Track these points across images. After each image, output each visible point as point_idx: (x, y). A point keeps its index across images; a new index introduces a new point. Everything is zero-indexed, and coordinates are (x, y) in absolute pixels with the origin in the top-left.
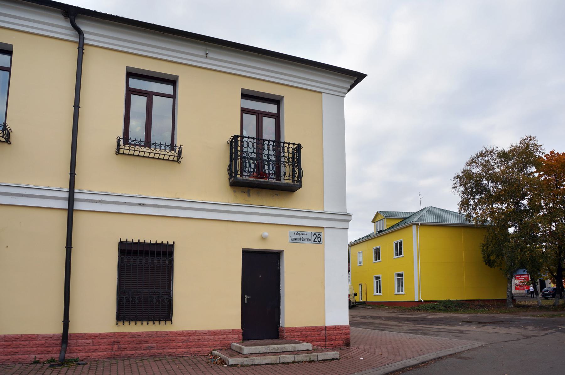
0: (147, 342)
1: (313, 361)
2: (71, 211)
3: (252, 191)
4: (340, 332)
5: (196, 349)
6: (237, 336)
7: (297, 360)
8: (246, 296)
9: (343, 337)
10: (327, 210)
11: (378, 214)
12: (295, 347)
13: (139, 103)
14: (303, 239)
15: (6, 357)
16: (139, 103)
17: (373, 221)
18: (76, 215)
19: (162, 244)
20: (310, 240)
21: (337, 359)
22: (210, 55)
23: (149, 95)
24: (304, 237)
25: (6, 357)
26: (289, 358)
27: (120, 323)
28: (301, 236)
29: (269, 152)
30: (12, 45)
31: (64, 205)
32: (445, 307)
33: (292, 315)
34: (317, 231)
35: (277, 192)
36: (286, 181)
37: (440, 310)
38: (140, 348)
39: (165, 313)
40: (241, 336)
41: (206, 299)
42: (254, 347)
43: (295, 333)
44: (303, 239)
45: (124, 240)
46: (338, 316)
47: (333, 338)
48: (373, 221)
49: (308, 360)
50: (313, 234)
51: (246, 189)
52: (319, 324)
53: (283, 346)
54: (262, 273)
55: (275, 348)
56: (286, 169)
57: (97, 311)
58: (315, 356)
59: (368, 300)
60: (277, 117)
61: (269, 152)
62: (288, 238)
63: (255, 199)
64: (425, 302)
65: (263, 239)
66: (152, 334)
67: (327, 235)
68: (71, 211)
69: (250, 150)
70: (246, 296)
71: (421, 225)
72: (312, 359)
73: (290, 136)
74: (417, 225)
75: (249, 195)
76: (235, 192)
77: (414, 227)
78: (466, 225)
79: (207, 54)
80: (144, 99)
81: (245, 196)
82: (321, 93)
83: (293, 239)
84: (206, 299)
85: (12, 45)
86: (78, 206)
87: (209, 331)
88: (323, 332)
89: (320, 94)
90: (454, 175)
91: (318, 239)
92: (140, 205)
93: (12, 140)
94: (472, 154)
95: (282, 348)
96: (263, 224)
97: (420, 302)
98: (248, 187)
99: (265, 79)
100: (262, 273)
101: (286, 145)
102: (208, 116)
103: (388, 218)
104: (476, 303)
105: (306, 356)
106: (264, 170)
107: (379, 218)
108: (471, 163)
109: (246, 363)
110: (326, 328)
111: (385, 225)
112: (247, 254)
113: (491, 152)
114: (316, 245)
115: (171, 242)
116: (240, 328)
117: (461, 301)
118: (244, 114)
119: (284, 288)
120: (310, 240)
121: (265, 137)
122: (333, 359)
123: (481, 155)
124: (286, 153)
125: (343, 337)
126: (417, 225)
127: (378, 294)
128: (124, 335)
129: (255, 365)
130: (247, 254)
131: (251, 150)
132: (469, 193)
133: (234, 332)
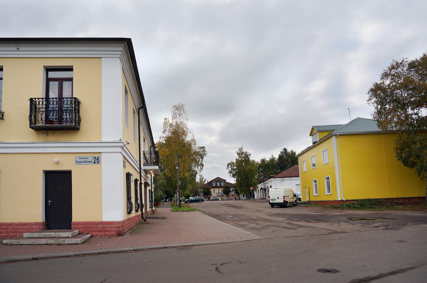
1: (61, 244)
3: (49, 132)
5: (12, 234)
6: (38, 226)
7: (48, 243)
8: (49, 201)
10: (104, 140)
11: (312, 129)
12: (59, 235)
14: (86, 162)
17: (310, 135)
20: (91, 162)
21: (79, 244)
22: (21, 49)
24: (86, 160)
26: (44, 241)
28: (84, 160)
29: (53, 105)
30: (130, 39)
32: (361, 205)
33: (80, 213)
34: (96, 156)
35: (67, 131)
37: (354, 207)
43: (79, 226)
44: (86, 162)
47: (108, 230)
48: (310, 135)
49: (57, 243)
50: (93, 157)
51: (46, 131)
53: (51, 233)
55: (44, 235)
58: (62, 241)
59: (311, 200)
61: (53, 105)
62: (74, 162)
63: (51, 137)
64: (346, 201)
67: (104, 158)
69: (41, 106)
70: (49, 201)
71: (339, 135)
72: (59, 243)
74: (336, 135)
75: (48, 135)
76: (38, 134)
77: (334, 138)
78: (380, 131)
79: (18, 48)
81: (45, 136)
82: (101, 58)
83: (78, 162)
85: (130, 39)
87: (20, 223)
89: (100, 59)
90: (369, 89)
91: (97, 160)
94: (385, 67)
95: (50, 235)
96: (58, 153)
97: (343, 201)
98: (47, 130)
99: (58, 57)
101: (65, 99)
103: (320, 132)
104: (395, 201)
105: (55, 241)
107: (315, 132)
108: (385, 75)
109: (14, 243)
110: (102, 223)
111: (317, 138)
112: (48, 174)
113: (401, 63)
114: (96, 165)
117: (380, 199)
118: (57, 83)
119: (43, 197)
120: (91, 162)
122: (76, 244)
123: (393, 67)
125: (116, 229)
126: (336, 135)
127: (329, 194)
129: (20, 244)
130: (48, 174)
131: (55, 106)
132: (381, 102)
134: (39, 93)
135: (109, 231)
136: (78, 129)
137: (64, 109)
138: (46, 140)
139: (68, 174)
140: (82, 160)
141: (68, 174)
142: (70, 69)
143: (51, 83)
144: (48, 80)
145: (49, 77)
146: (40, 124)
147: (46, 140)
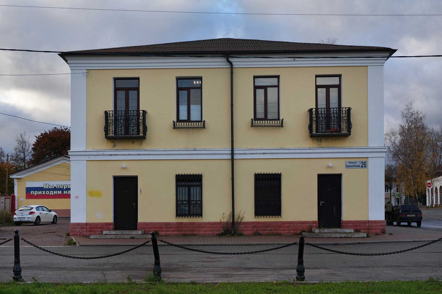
0: (269, 227)
2: (232, 160)
4: (378, 224)
9: (380, 227)
10: (370, 145)
13: (260, 92)
14: (355, 166)
15: (210, 232)
16: (260, 92)
18: (235, 162)
19: (275, 174)
20: (359, 166)
23: (265, 88)
24: (355, 164)
25: (210, 232)
27: (257, 217)
28: (353, 164)
31: (229, 157)
33: (348, 214)
34: (364, 160)
36: (344, 132)
38: (266, 230)
39: (278, 212)
40: (318, 225)
41: (300, 205)
42: (220, 35)
44: (355, 166)
45: (257, 173)
46: (378, 214)
52: (365, 219)
54: (330, 188)
56: (344, 125)
57: (247, 211)
60: (339, 87)
63: (324, 144)
65: (329, 167)
66: (186, 224)
67: (370, 163)
68: (232, 160)
69: (112, 118)
73: (345, 105)
76: (313, 140)
80: (186, 92)
83: (347, 166)
84: (300, 205)
86: (236, 157)
88: (367, 224)
89: (366, 67)
91: (364, 165)
92: (264, 153)
93: (206, 126)
96: (330, 158)
100: (330, 188)
102: (298, 93)
106: (330, 124)
110: (369, 222)
112: (321, 177)
115: (279, 173)
116: (317, 220)
120: (359, 166)
121: (331, 106)
124: (344, 115)
125: (380, 227)
128: (181, 223)
130: (321, 177)
133: (314, 222)
134: (110, 107)
135: (375, 229)
136: (144, 138)
137: (110, 122)
138: (319, 146)
139: (339, 177)
140: (351, 165)
141: (339, 177)
142: (200, 79)
143: (257, 90)
144: (256, 88)
145: (130, 92)
146: (111, 135)
147: (319, 146)
